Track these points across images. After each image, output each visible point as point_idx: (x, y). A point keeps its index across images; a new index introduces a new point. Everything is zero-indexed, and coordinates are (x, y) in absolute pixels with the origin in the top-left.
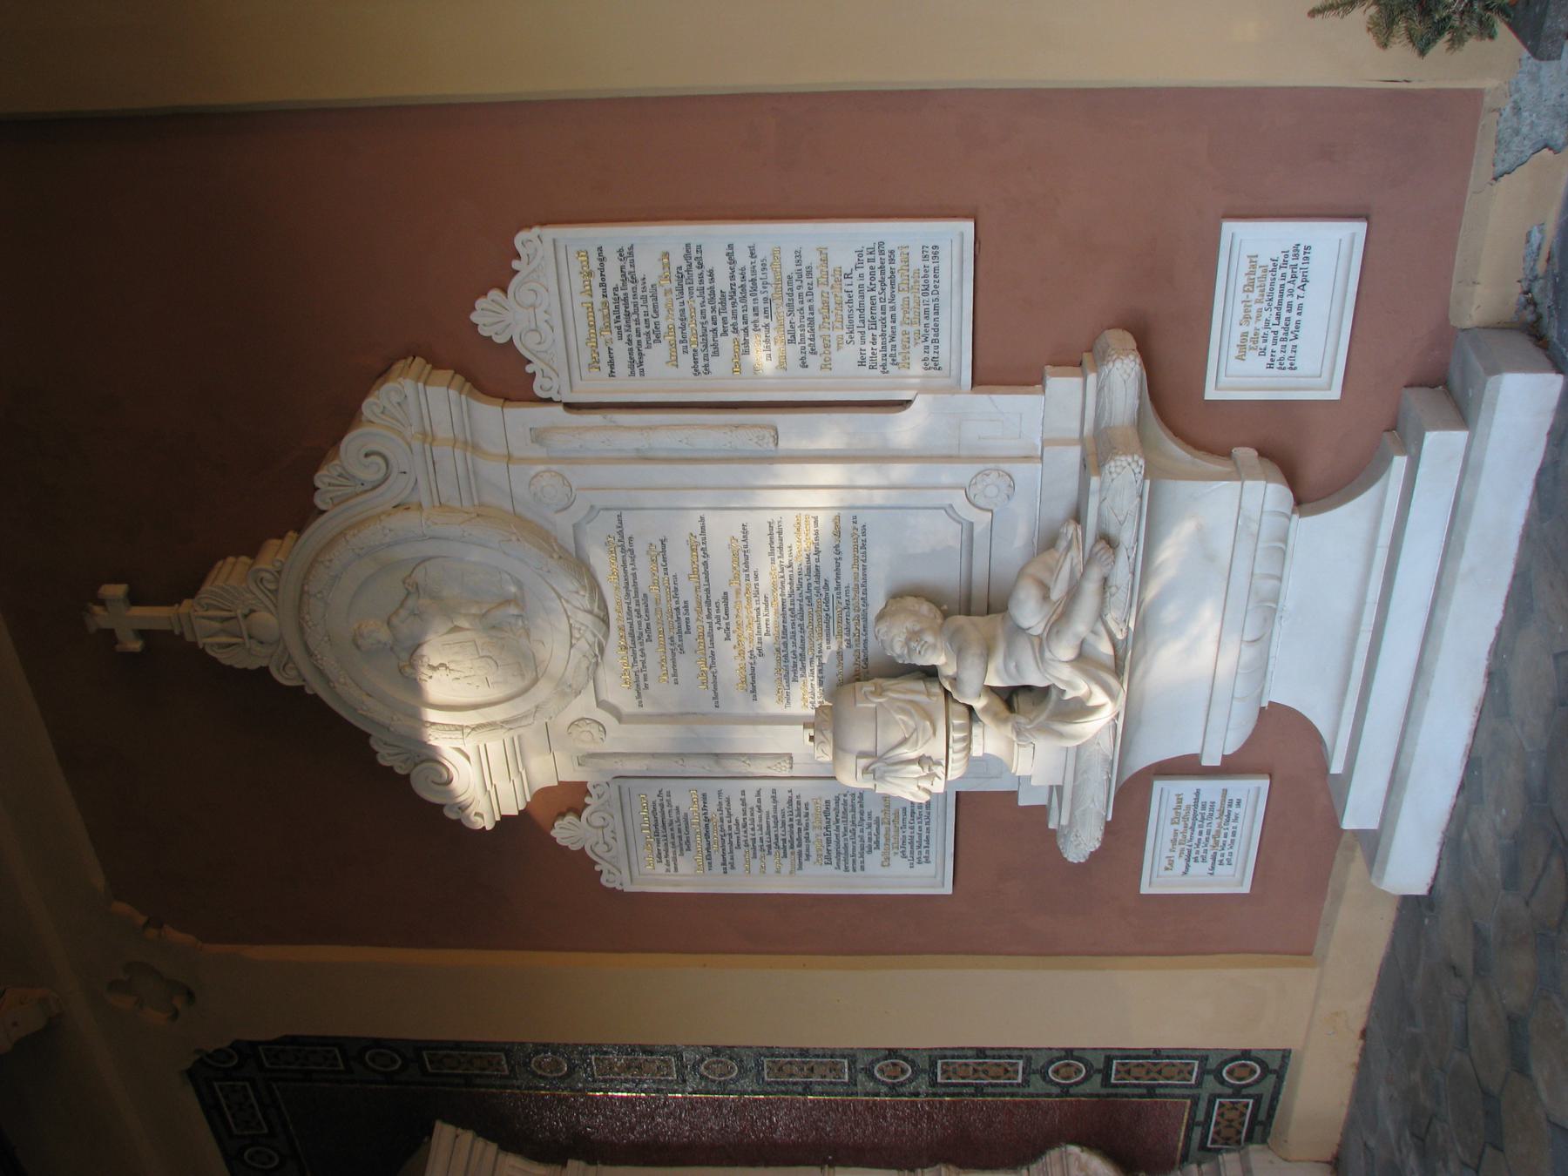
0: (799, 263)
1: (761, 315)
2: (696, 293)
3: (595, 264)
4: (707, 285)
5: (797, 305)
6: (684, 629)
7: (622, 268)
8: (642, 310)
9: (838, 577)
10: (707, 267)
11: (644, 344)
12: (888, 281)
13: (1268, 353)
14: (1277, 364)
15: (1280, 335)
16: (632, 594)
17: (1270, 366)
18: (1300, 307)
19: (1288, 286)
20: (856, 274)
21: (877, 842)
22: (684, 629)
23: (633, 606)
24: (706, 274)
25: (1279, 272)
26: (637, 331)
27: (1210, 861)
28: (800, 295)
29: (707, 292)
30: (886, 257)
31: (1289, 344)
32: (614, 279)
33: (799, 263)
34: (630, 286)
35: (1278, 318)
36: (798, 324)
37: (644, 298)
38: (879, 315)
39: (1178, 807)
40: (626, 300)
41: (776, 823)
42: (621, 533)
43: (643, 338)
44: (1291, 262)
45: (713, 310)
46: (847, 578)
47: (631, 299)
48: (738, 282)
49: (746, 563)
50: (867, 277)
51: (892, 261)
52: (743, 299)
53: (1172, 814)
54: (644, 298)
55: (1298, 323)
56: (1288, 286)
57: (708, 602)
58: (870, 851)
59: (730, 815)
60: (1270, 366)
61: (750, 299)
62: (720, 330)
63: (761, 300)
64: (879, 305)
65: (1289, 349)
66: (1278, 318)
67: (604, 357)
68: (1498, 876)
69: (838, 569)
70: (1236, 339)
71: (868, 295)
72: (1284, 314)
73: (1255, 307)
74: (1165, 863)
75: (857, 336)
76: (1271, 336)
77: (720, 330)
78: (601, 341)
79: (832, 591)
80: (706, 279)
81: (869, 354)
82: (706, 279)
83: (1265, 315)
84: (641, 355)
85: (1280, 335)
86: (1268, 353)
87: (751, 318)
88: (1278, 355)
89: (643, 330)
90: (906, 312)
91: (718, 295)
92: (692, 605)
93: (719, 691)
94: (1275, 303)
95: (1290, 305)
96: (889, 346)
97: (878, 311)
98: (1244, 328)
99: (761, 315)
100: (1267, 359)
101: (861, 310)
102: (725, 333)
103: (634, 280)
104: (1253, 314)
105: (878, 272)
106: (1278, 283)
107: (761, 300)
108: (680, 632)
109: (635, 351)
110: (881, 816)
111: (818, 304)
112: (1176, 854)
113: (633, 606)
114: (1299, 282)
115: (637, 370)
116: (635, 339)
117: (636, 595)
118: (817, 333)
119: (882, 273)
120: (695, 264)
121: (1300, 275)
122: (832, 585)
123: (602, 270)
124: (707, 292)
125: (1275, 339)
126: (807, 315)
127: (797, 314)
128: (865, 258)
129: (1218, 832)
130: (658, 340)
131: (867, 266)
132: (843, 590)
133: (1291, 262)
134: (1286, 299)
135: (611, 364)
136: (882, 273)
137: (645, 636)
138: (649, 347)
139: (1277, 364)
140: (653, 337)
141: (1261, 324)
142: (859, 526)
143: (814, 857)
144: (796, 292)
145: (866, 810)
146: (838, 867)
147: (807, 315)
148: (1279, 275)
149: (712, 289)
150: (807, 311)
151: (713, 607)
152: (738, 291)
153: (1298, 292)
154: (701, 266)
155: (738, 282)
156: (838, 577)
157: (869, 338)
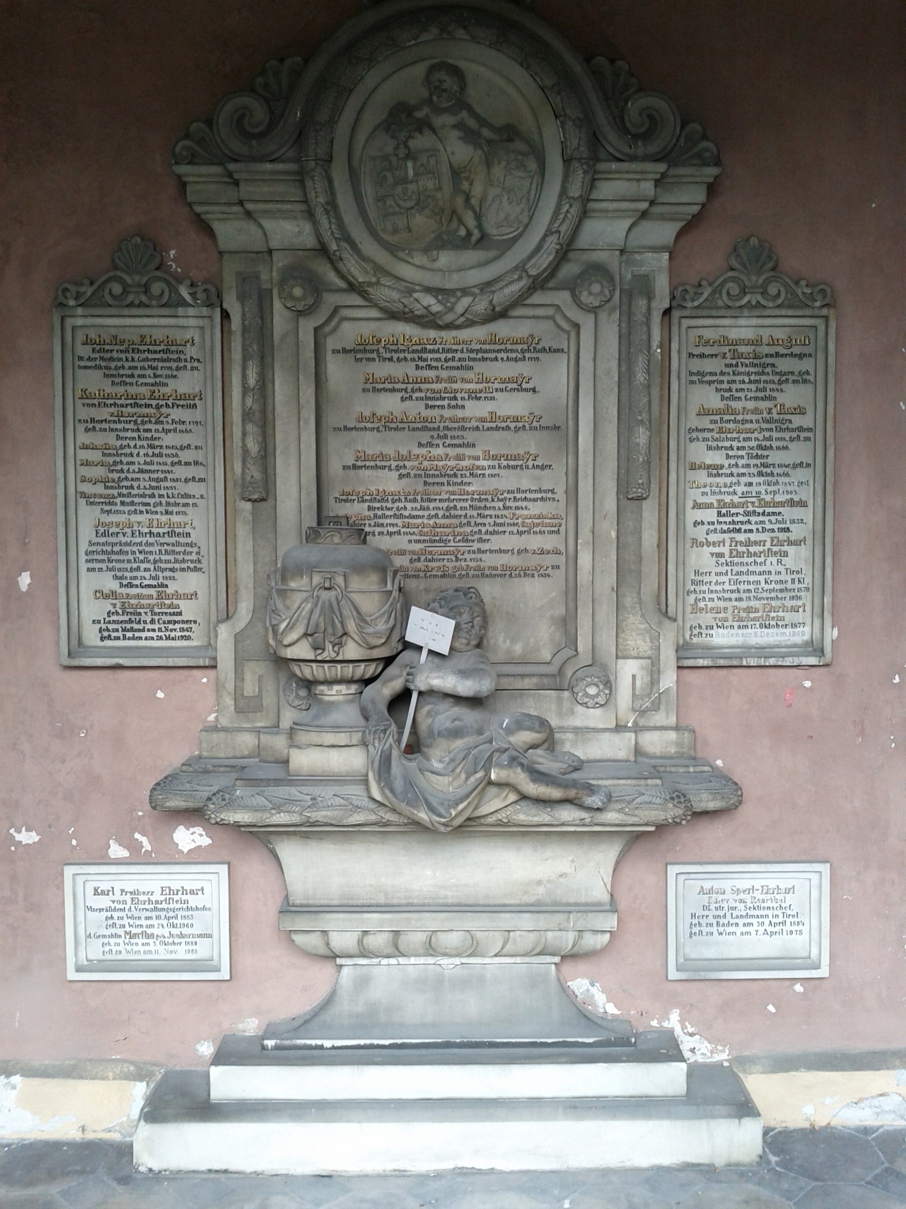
0: (793, 522)
1: (745, 489)
2: (767, 434)
3: (796, 350)
4: (775, 444)
5: (753, 519)
6: (430, 403)
7: (792, 373)
8: (753, 387)
9: (491, 551)
10: (790, 445)
11: (719, 386)
12: (773, 595)
13: (706, 913)
14: (695, 921)
15: (722, 921)
16: (473, 355)
17: (693, 916)
18: (749, 933)
19: (767, 921)
20: (781, 568)
21: (130, 585)
22: (430, 403)
23: (458, 355)
24: (785, 444)
25: (779, 913)
26: (734, 382)
27: (108, 932)
28: (762, 522)
29: (768, 443)
30: (796, 593)
31: (714, 929)
32: (784, 365)
33: (793, 522)
34: (776, 378)
35: (737, 917)
36: (736, 519)
37: (765, 390)
38: (742, 587)
39: (184, 891)
40: (763, 373)
41: (157, 480)
42: (544, 350)
43: (725, 386)
44: (788, 921)
45: (752, 448)
46: (489, 560)
47: (764, 378)
48: (777, 471)
49: (508, 467)
50: (778, 578)
51: (792, 598)
52: (760, 474)
53: (175, 886)
54: (765, 390)
55: (734, 933)
56: (767, 921)
57: (463, 429)
58: (116, 577)
59: (167, 431)
60: (693, 916)
61: (761, 479)
62: (731, 453)
63: (759, 489)
64: (752, 587)
65: (709, 929)
66: (737, 917)
67: (707, 351)
68: (747, 1053)
69: (501, 551)
70: (717, 885)
71: (762, 578)
72: (741, 922)
73: (747, 897)
74: (105, 886)
75: (723, 569)
76: (721, 913)
77: (731, 453)
78: (726, 349)
79: (476, 546)
80: (780, 444)
81: (706, 579)
82: (780, 444)
83: (741, 906)
84: (710, 383)
85: (722, 921)
86: (706, 913)
87: (744, 480)
88: (704, 921)
89: (734, 387)
90: (745, 610)
91: (765, 453)
92: (459, 413)
93: (354, 433)
94: (752, 912)
95: (751, 924)
96: (714, 596)
97: (747, 587)
98: (728, 890)
99: (745, 489)
100: (700, 912)
101: (748, 573)
102: (728, 457)
103: (780, 382)
104: (742, 896)
105: (783, 586)
106: (770, 913)
107: (759, 489)
108: (428, 398)
109: (714, 378)
110: (169, 591)
111: (753, 537)
112: (118, 896)
113: (458, 355)
114: (770, 929)
115: (695, 378)
116: (725, 378)
117: (471, 359)
118: (727, 536)
119: (781, 591)
120: (794, 435)
121: (777, 929)
122: (485, 546)
123: (791, 355)
124: (768, 443)
125: (719, 916)
126: (744, 527)
127: (746, 519)
128: (795, 576)
129: (149, 936)
130: (723, 398)
131: (789, 578)
132: (479, 556)
133: (788, 921)
134: (754, 921)
135: (702, 356)
136: (781, 591)
137: (421, 364)
138: (717, 390)
139: (695, 921)
140: (727, 395)
141: (732, 904)
142: (549, 571)
143: (106, 519)
144: (766, 519)
145: (177, 575)
146: (91, 543)
147: (744, 527)
148: (776, 912)
149: (771, 447)
150: (749, 527)
151: (457, 433)
152: (768, 470)
153: (761, 929)
154: (792, 440)
155: (777, 471)
156: (491, 551)
157: (721, 579)
